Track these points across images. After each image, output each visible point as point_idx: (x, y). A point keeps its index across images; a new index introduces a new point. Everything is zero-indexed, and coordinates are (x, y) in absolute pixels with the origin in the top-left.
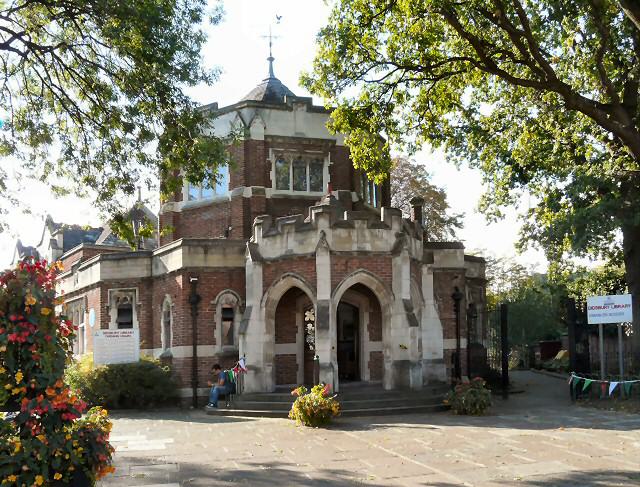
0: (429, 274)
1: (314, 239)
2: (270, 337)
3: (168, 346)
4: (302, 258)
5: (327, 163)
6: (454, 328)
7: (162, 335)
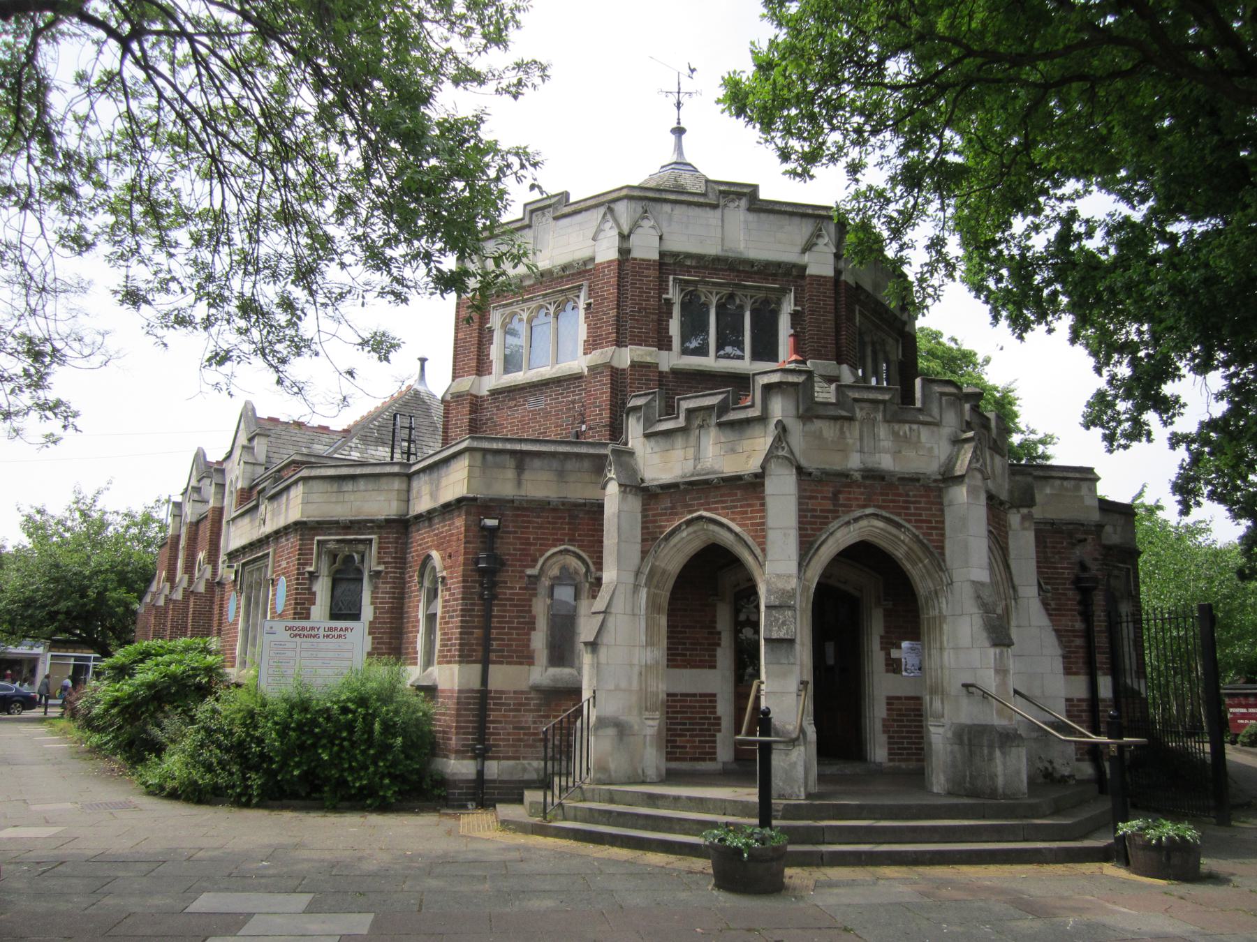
0: (1024, 529)
1: (759, 444)
2: (658, 653)
3: (428, 662)
4: (733, 483)
5: (788, 307)
6: (1081, 653)
7: (419, 636)
